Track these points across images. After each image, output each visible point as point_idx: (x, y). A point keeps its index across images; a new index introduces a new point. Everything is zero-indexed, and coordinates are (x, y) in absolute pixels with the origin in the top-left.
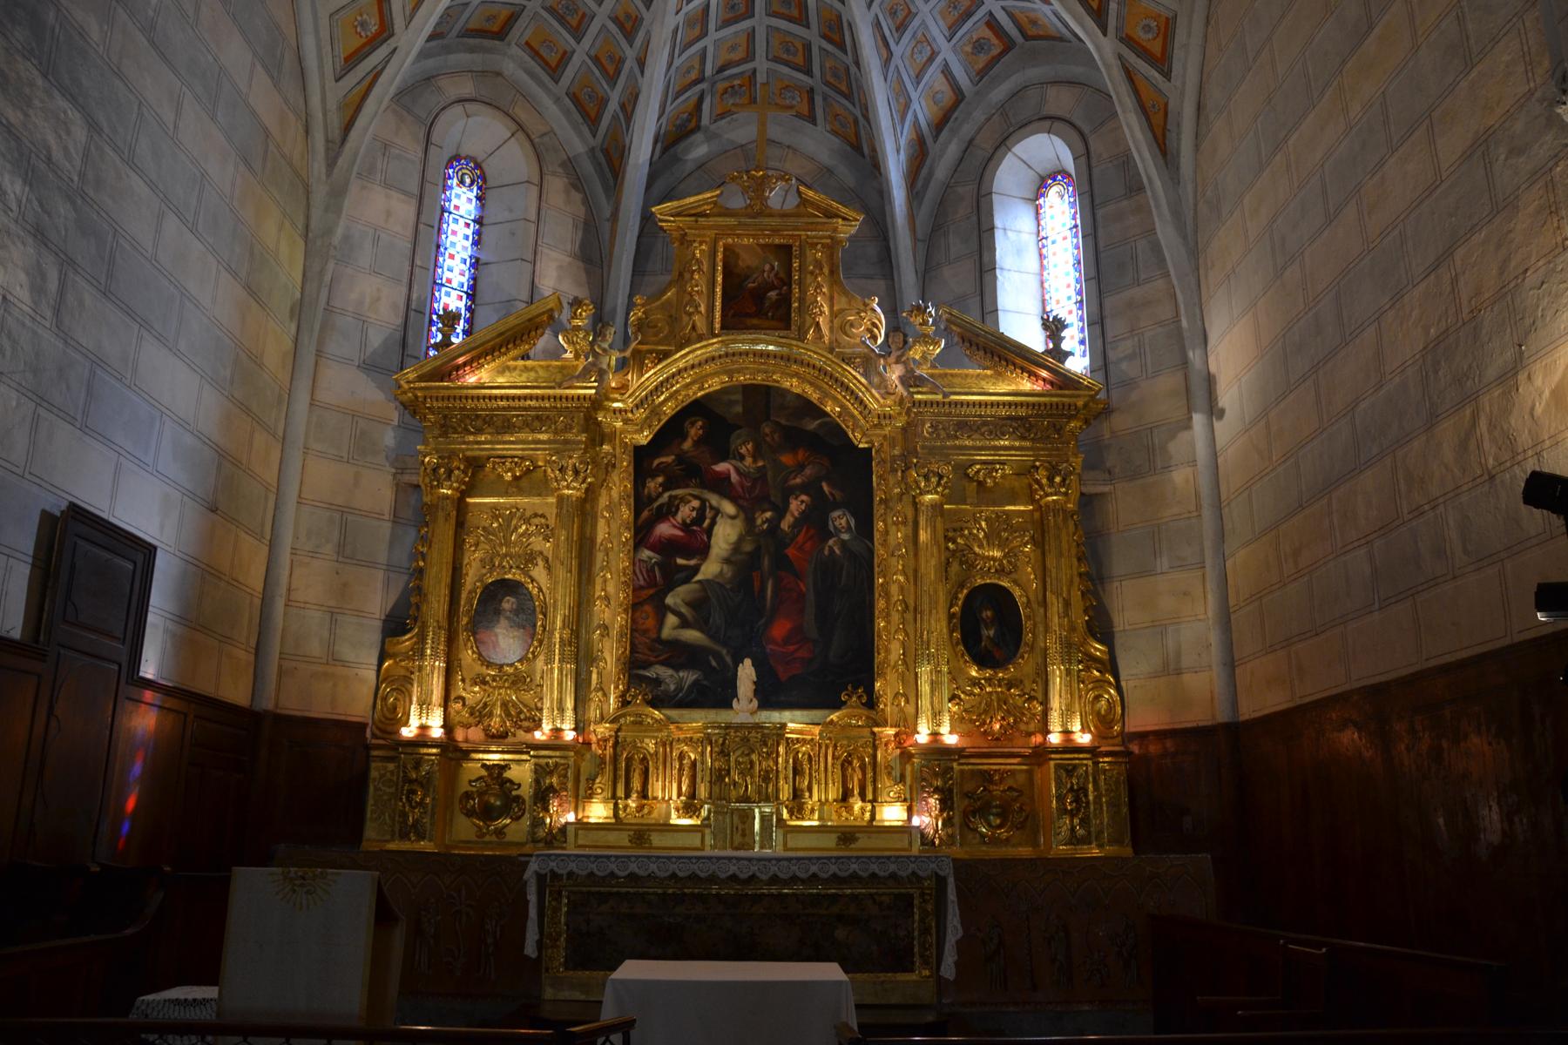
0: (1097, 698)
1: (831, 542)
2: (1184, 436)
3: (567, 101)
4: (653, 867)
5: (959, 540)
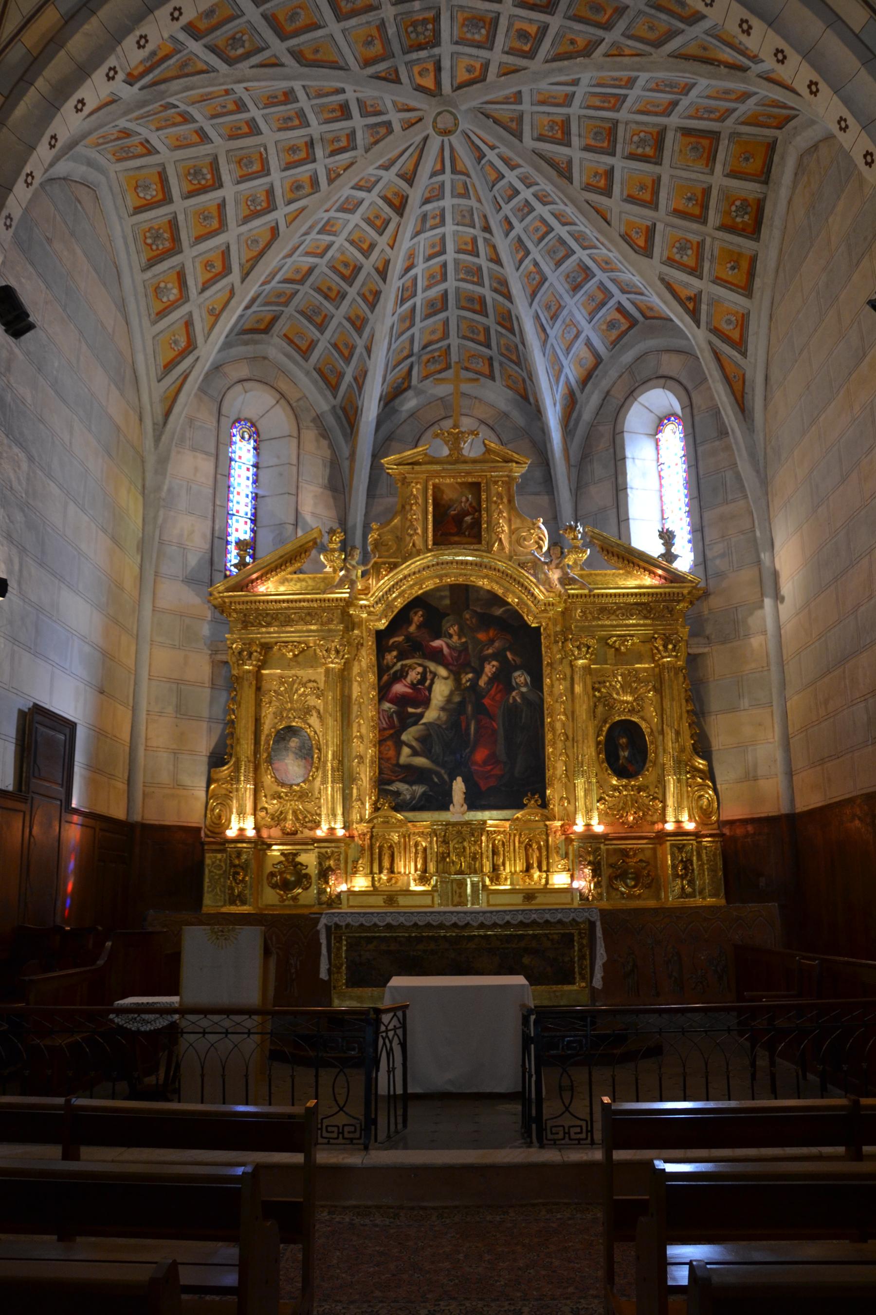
0: (701, 797)
1: (514, 694)
2: (758, 613)
3: (315, 375)
4: (402, 919)
5: (603, 690)
